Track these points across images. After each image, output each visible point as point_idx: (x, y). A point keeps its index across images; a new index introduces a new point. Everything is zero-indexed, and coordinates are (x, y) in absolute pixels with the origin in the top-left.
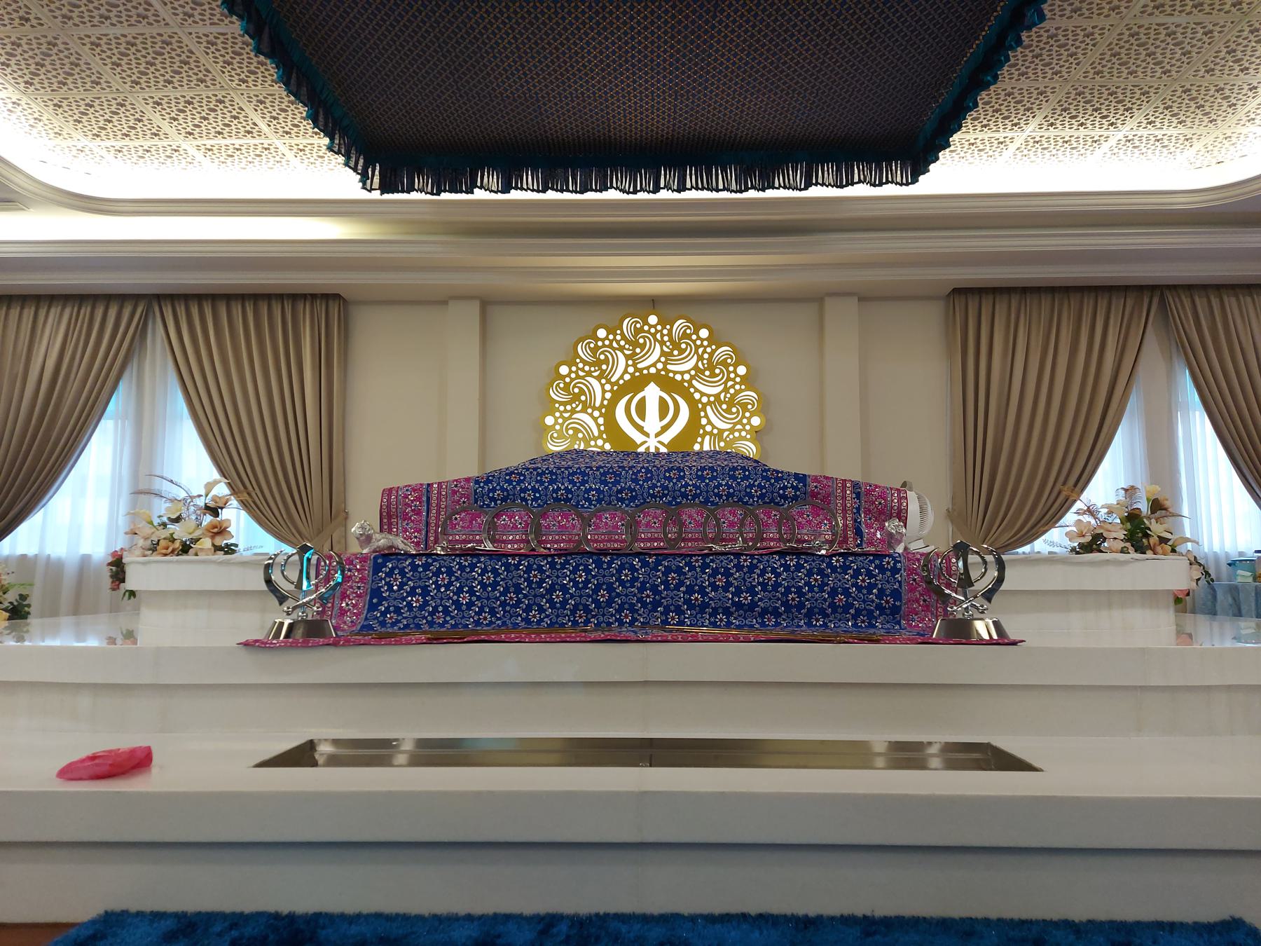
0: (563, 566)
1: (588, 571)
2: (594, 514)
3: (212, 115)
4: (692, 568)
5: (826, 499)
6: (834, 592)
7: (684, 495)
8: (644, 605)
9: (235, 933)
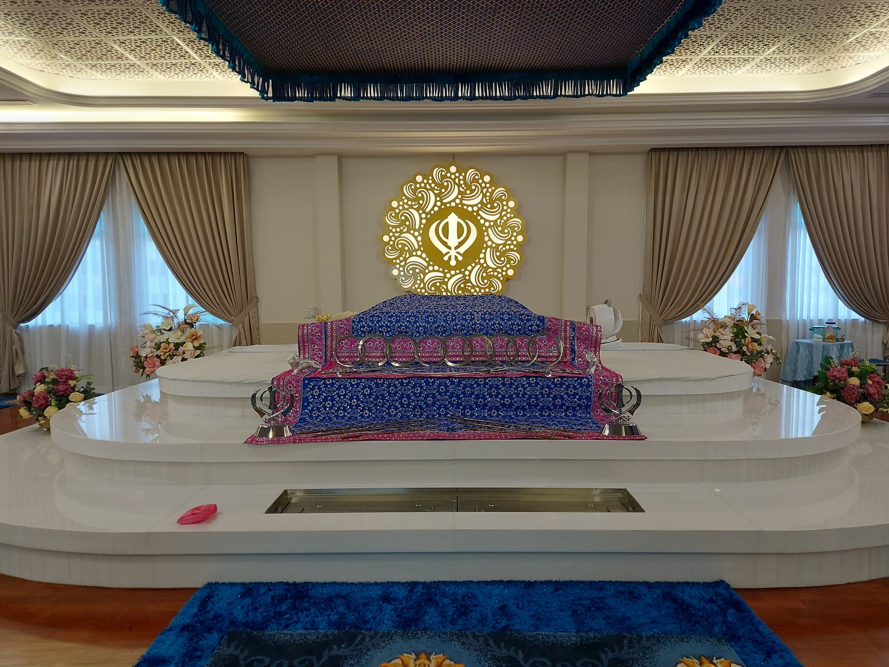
0: (407, 384)
1: (421, 387)
2: (421, 341)
3: (162, 56)
4: (479, 385)
5: (555, 332)
6: (555, 398)
7: (474, 330)
8: (452, 405)
9: (271, 593)
